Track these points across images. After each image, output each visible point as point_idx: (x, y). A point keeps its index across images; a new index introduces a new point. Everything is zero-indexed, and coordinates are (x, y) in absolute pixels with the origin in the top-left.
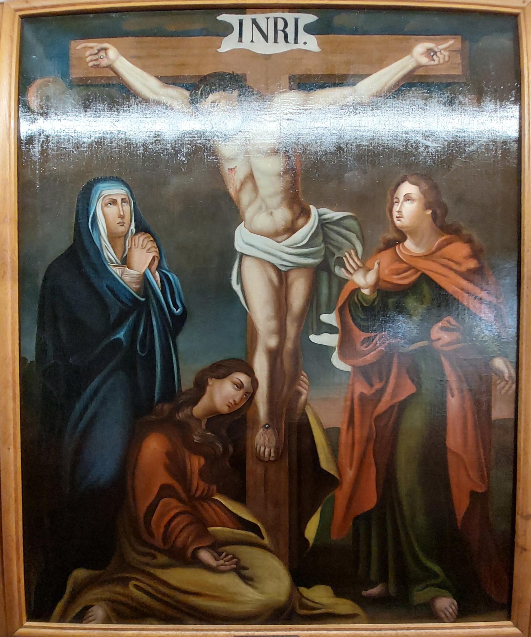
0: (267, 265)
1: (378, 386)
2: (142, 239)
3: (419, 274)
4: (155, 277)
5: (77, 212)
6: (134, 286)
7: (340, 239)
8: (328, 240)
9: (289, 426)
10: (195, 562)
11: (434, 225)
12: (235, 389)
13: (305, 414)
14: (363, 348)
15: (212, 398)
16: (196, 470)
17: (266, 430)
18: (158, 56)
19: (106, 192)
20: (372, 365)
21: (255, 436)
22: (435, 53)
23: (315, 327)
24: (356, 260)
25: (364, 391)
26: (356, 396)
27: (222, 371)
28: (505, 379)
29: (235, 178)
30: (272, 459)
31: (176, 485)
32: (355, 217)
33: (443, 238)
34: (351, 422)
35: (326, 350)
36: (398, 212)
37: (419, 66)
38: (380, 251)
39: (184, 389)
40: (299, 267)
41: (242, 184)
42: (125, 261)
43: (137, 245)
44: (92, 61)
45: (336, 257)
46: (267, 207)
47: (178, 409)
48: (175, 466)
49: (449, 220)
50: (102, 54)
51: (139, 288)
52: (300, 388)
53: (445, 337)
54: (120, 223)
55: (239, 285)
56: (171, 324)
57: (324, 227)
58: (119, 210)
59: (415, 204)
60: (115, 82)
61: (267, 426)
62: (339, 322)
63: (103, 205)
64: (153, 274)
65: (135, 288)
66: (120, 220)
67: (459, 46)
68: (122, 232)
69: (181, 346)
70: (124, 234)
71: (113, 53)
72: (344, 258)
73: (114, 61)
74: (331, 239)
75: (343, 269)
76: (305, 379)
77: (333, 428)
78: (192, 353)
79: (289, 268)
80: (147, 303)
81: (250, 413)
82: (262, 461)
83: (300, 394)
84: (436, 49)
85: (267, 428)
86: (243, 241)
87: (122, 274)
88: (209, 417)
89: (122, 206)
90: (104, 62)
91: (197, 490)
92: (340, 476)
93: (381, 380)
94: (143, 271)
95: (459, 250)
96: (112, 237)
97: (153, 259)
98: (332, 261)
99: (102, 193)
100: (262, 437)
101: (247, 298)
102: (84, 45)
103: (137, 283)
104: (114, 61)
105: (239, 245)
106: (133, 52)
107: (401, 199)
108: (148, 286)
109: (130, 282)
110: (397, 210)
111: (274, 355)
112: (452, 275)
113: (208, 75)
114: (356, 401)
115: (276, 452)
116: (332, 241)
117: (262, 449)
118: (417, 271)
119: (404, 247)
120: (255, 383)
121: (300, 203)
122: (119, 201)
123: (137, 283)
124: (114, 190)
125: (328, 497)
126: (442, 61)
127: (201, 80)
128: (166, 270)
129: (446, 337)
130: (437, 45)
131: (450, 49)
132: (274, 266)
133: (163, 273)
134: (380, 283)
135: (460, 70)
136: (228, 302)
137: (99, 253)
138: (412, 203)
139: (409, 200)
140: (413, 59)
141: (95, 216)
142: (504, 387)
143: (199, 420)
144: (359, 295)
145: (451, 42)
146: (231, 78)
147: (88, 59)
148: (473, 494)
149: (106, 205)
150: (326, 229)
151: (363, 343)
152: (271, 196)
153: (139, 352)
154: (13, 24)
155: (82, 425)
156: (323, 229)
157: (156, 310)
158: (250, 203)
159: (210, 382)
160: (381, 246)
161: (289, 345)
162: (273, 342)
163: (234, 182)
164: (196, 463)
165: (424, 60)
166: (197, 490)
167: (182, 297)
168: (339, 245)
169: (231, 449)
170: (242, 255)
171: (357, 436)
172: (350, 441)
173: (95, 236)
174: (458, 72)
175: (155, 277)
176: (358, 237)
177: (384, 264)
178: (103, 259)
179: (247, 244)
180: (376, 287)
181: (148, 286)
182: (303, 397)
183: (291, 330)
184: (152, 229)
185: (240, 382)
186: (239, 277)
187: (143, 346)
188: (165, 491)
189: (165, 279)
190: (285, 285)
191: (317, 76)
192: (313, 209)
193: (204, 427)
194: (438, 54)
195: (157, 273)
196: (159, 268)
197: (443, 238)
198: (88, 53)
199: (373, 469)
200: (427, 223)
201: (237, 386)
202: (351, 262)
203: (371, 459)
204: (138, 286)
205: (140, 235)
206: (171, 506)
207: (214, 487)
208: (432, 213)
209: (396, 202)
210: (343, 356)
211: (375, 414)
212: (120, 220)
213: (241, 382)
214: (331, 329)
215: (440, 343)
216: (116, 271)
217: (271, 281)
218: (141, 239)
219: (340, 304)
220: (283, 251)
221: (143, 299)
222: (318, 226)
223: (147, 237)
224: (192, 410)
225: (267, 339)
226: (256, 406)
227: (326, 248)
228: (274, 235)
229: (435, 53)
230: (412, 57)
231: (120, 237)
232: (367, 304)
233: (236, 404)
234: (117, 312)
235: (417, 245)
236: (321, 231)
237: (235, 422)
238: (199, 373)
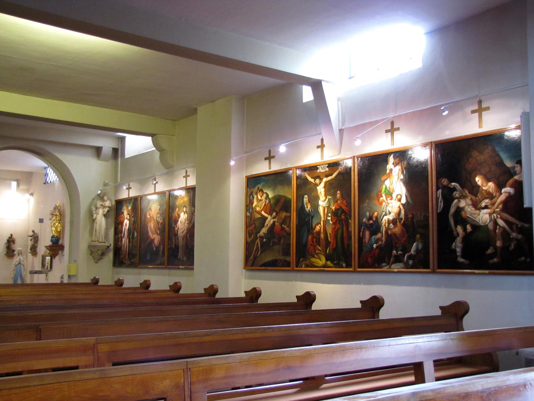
10: (314, 257)
35: (329, 220)
78: (315, 222)
105: (320, 204)
111: (323, 221)
136: (318, 212)
154: (351, 348)
164: (315, 240)
180: (335, 209)
206: (312, 247)
225: (323, 219)
237: (319, 233)
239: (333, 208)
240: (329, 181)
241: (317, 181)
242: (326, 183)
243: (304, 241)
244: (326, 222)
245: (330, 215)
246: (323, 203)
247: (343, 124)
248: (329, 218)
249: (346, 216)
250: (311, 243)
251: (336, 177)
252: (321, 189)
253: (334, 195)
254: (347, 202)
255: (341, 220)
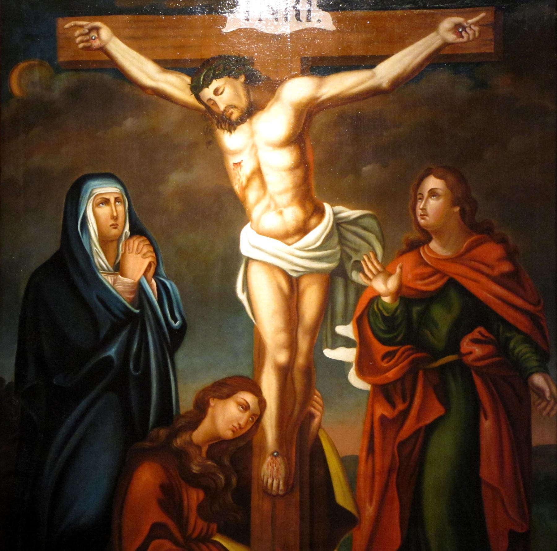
0: (276, 271)
1: (401, 407)
2: (137, 243)
3: (446, 279)
4: (151, 286)
5: (65, 212)
6: (128, 296)
7: (358, 240)
8: (344, 242)
9: (300, 452)
11: (463, 223)
12: (241, 411)
13: (317, 440)
14: (384, 364)
15: (214, 422)
16: (194, 504)
17: (274, 459)
18: (155, 37)
19: (98, 191)
20: (394, 383)
21: (262, 465)
22: (464, 29)
23: (330, 340)
24: (376, 264)
25: (386, 413)
26: (377, 417)
27: (226, 390)
28: (547, 400)
29: (241, 173)
30: (281, 493)
31: (171, 524)
32: (374, 215)
33: (474, 238)
34: (371, 450)
35: (341, 367)
36: (422, 209)
37: (446, 44)
38: (402, 253)
39: (183, 411)
40: (311, 272)
41: (249, 180)
42: (118, 268)
43: (131, 250)
44: (82, 42)
45: (352, 261)
46: (276, 206)
47: (175, 434)
48: (170, 499)
49: (478, 218)
50: (94, 34)
51: (133, 299)
52: (313, 409)
53: (477, 350)
54: (113, 225)
55: (245, 293)
56: (169, 340)
57: (340, 228)
58: (112, 210)
59: (441, 201)
60: (108, 66)
61: (275, 454)
62: (357, 334)
63: (94, 205)
64: (149, 283)
65: (128, 298)
66: (112, 222)
67: (491, 19)
68: (115, 236)
69: (180, 365)
70: (117, 238)
71: (105, 33)
72: (362, 262)
73: (107, 43)
74: (348, 240)
75: (361, 275)
76: (318, 399)
77: (351, 457)
79: (300, 274)
80: (142, 315)
81: (256, 439)
82: (270, 495)
83: (312, 416)
84: (465, 24)
85: (276, 457)
86: (250, 244)
87: (115, 282)
88: (210, 443)
89: (115, 206)
90: (96, 44)
91: (194, 529)
92: (359, 512)
93: (404, 401)
94: (137, 279)
95: (491, 252)
96: (104, 241)
97: (150, 265)
98: (349, 265)
99: (94, 192)
100: (270, 467)
101: (254, 304)
102: (72, 23)
103: (131, 293)
104: (107, 43)
105: (245, 249)
106: (128, 32)
107: (426, 194)
108: (143, 297)
109: (123, 292)
110: (421, 207)
111: (285, 373)
112: (484, 280)
113: (212, 58)
114: (376, 424)
115: (286, 483)
116: (348, 243)
117: (270, 481)
118: (444, 275)
119: (428, 247)
120: (262, 403)
121: (312, 200)
122: (112, 201)
123: (131, 293)
124: (106, 189)
125: (342, 540)
126: (471, 37)
127: (203, 64)
128: (164, 277)
129: (478, 351)
130: (467, 19)
131: (481, 23)
132: (284, 272)
133: (160, 281)
134: (404, 290)
135: (492, 46)
136: (234, 314)
137: (88, 258)
138: (438, 199)
139: (434, 196)
140: (439, 37)
141: (85, 217)
142: (545, 408)
143: (199, 447)
144: (379, 303)
145: (483, 15)
146: (237, 61)
147: (79, 39)
148: (512, 534)
149: (98, 205)
150: (342, 229)
151: (384, 357)
152: (281, 193)
153: (133, 372)
155: (73, 441)
156: (338, 229)
157: (152, 323)
158: (258, 201)
159: (212, 403)
160: (404, 247)
161: (301, 361)
162: (282, 357)
163: (240, 177)
164: (194, 497)
165: (451, 38)
166: (194, 529)
167: (182, 308)
168: (357, 248)
169: (234, 480)
170: (248, 260)
171: (378, 466)
172: (369, 472)
173: (85, 240)
174: (489, 49)
175: (151, 286)
176: (377, 238)
177: (407, 268)
178: (93, 266)
179: (254, 247)
180: (399, 294)
181: (143, 297)
182: (316, 420)
183: (303, 344)
184: (149, 232)
185: (246, 404)
186: (245, 284)
187: (136, 368)
188: (157, 531)
189: (162, 288)
190: (296, 294)
191: (332, 58)
192: (328, 207)
193: (204, 454)
194: (468, 30)
195: (153, 281)
196: (156, 275)
197: (474, 238)
198: (77, 33)
199: (397, 504)
200: (454, 222)
201: (243, 408)
202: (370, 266)
203: (393, 493)
204: (132, 296)
205: (134, 238)
207: (214, 526)
208: (460, 210)
209: (420, 199)
210: (362, 373)
211: (398, 440)
212: (112, 222)
213: (247, 403)
214: (347, 343)
215: (470, 358)
216: (108, 279)
217: (280, 289)
218: (136, 243)
219: (358, 314)
220: (295, 255)
221: (137, 311)
222: (333, 226)
223: (143, 241)
224: (191, 434)
225: (276, 354)
226: (263, 430)
227: (342, 251)
228: (285, 237)
229: (464, 29)
230: (438, 34)
231: (112, 241)
232: (388, 313)
233: (241, 428)
234: (108, 326)
235: (444, 246)
236: (336, 231)
237: (241, 448)
238: (199, 393)
239: (384, 287)
240: (336, 101)
241: (225, 93)
242: (308, 115)
243: (87, 501)
244: (306, 379)
245: (346, 330)
246: (276, 244)
247: (302, 67)
248: (346, 355)
249: (502, 348)
250: (156, 515)
251: (400, 83)
252: (260, 151)
253: (391, 202)
254: (510, 255)
255: (462, 369)
